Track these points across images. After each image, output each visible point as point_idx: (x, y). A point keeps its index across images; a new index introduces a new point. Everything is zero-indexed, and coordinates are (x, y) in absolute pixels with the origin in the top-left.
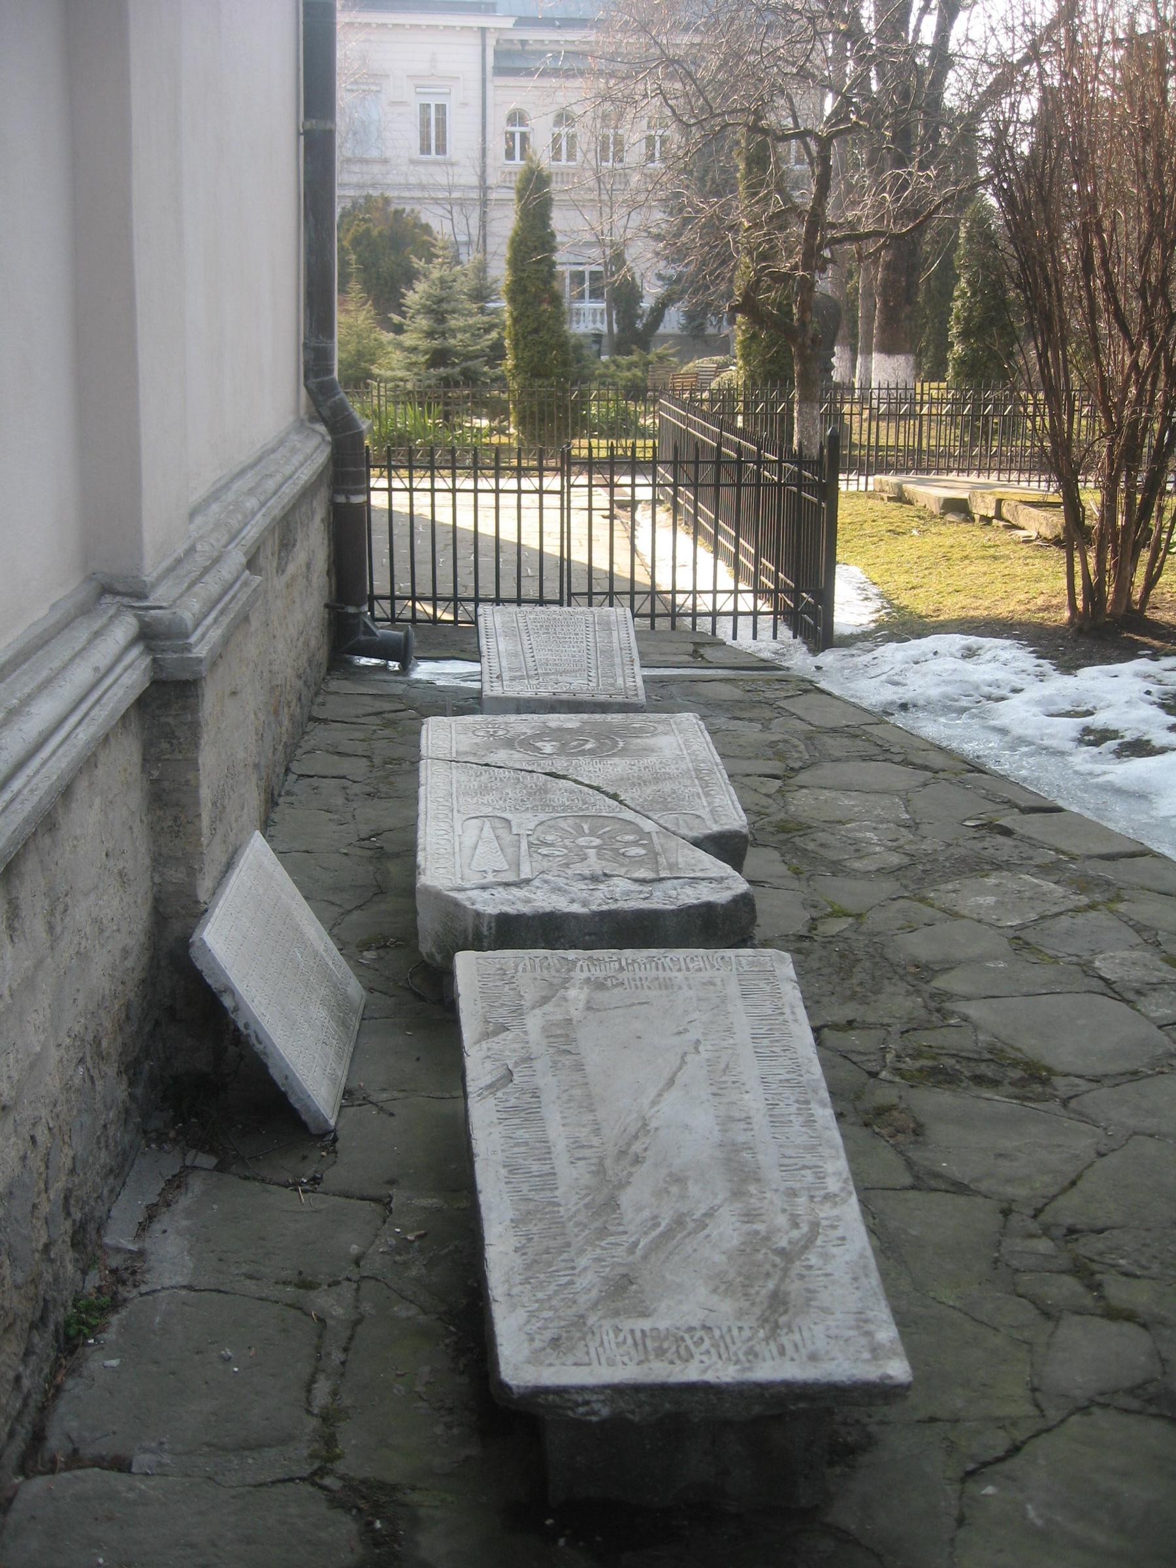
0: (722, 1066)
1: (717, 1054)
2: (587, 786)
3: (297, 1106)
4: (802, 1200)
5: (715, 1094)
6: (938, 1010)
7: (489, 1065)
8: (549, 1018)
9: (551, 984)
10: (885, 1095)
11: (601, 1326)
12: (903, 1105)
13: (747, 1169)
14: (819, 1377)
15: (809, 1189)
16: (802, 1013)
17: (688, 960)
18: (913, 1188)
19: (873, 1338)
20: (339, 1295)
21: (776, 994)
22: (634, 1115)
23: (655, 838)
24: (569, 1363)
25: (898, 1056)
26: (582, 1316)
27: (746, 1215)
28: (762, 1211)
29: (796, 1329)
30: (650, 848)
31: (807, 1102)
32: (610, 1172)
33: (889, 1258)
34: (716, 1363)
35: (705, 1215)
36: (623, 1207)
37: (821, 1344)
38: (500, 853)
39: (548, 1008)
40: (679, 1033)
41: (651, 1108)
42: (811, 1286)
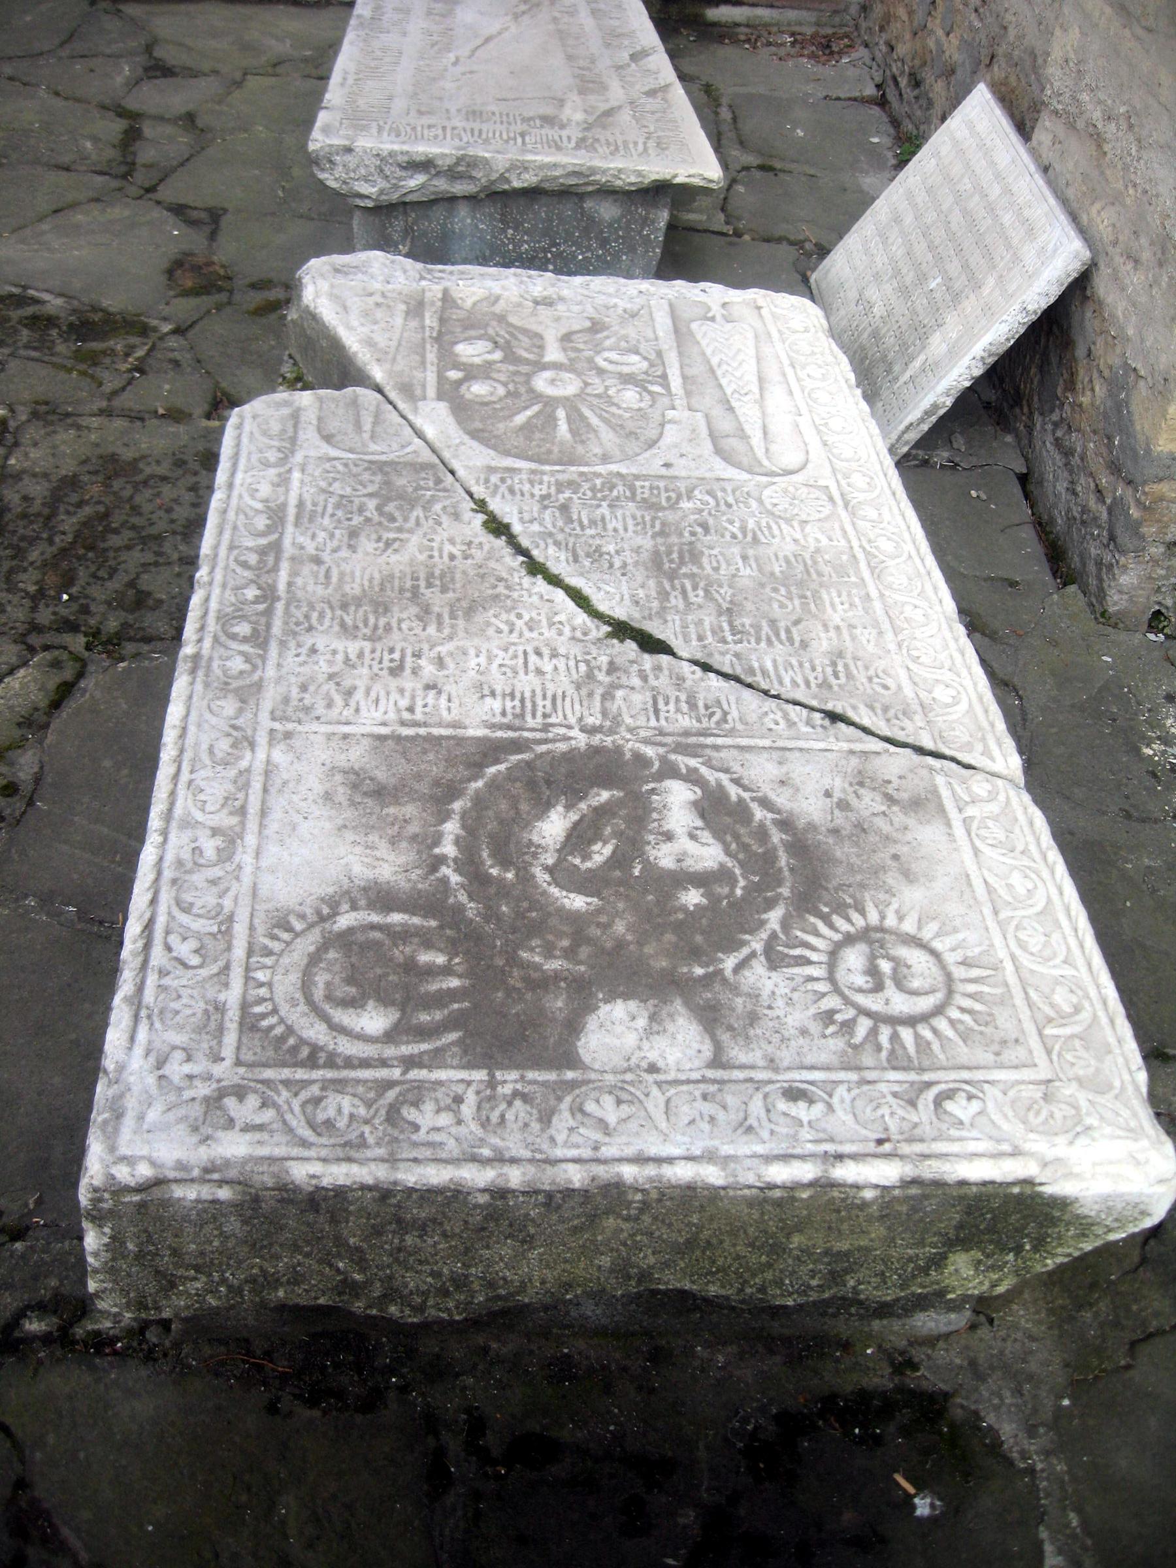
2: (555, 581)
7: (652, 67)
23: (431, 377)
30: (448, 359)
38: (714, 361)
39: (604, 107)
40: (471, 72)
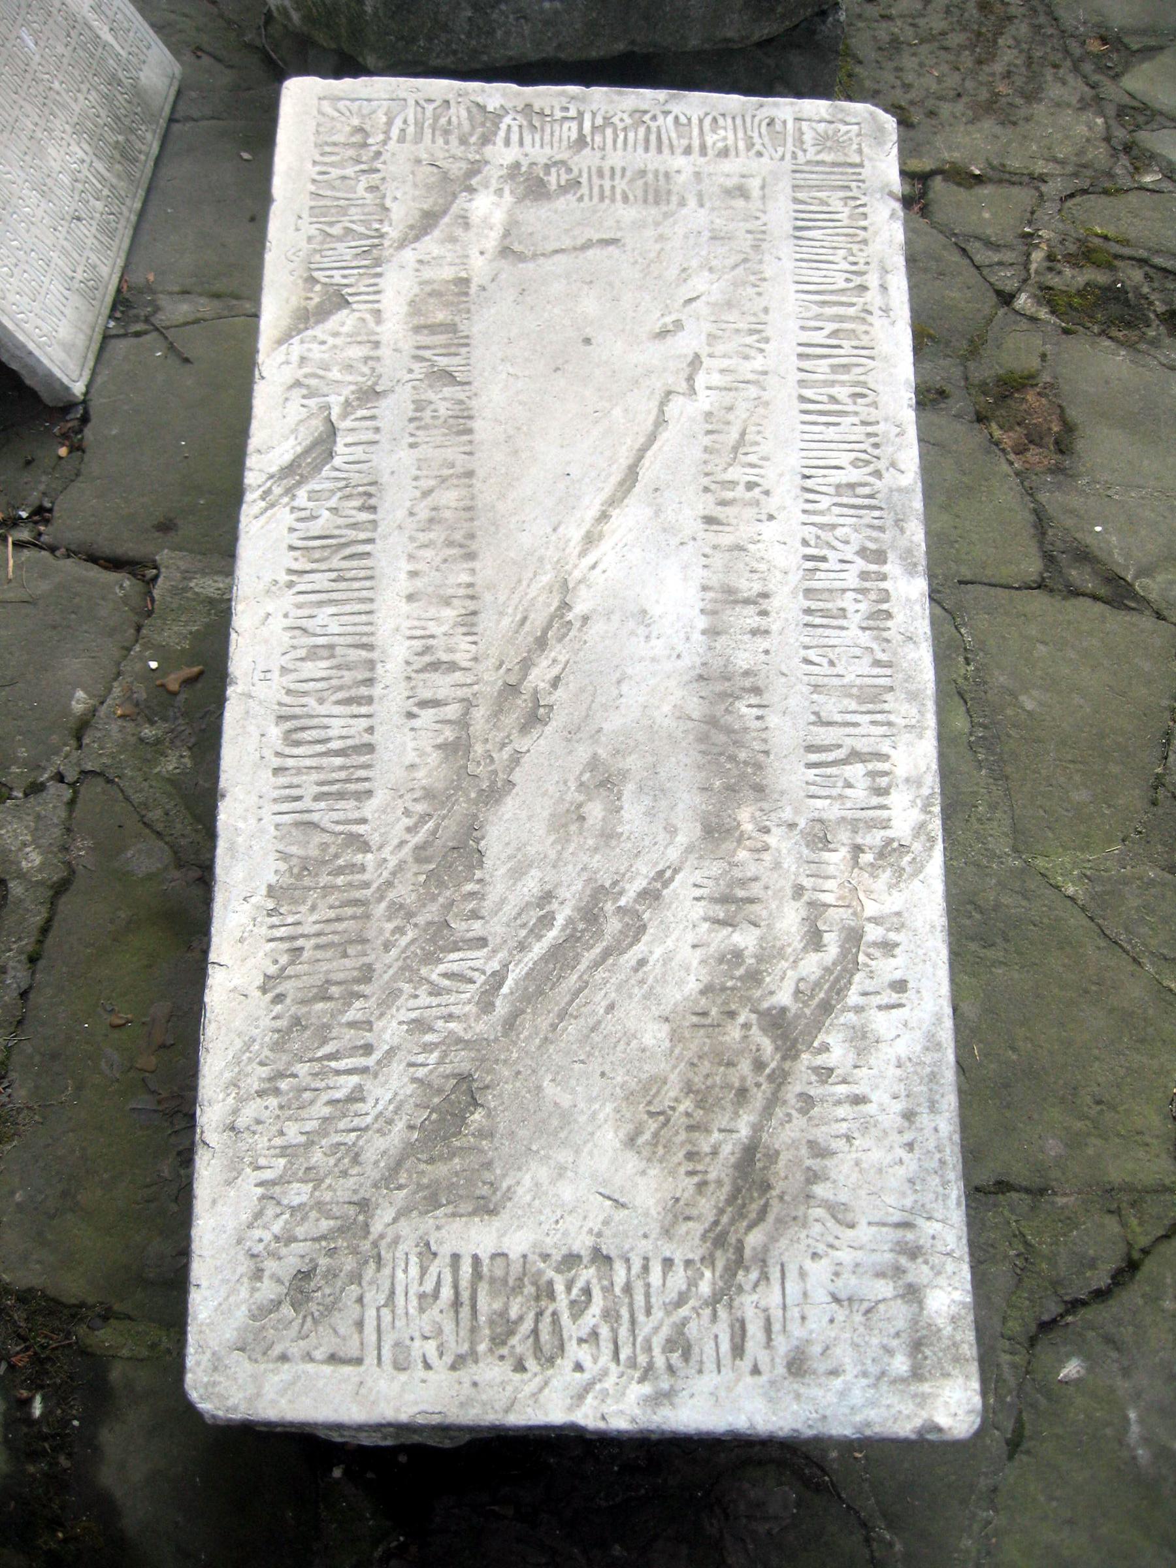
0: (735, 435)
1: (728, 398)
3: (14, 366)
4: (837, 858)
5: (710, 520)
6: (1128, 148)
8: (428, 273)
9: (445, 177)
10: (1018, 350)
11: (396, 1241)
12: (1046, 378)
13: (743, 755)
14: (799, 1426)
15: (854, 825)
16: (899, 284)
17: (707, 122)
18: (1040, 586)
19: (921, 1303)
20: (38, 817)
21: (858, 235)
22: (545, 579)
24: (318, 1354)
25: (1050, 258)
26: (364, 1205)
27: (725, 899)
28: (755, 890)
29: (775, 1273)
31: (880, 557)
32: (479, 749)
33: (980, 765)
34: (605, 1373)
35: (644, 894)
36: (488, 862)
37: (818, 1325)
39: (430, 245)
40: (663, 334)
41: (583, 553)
42: (820, 1134)
